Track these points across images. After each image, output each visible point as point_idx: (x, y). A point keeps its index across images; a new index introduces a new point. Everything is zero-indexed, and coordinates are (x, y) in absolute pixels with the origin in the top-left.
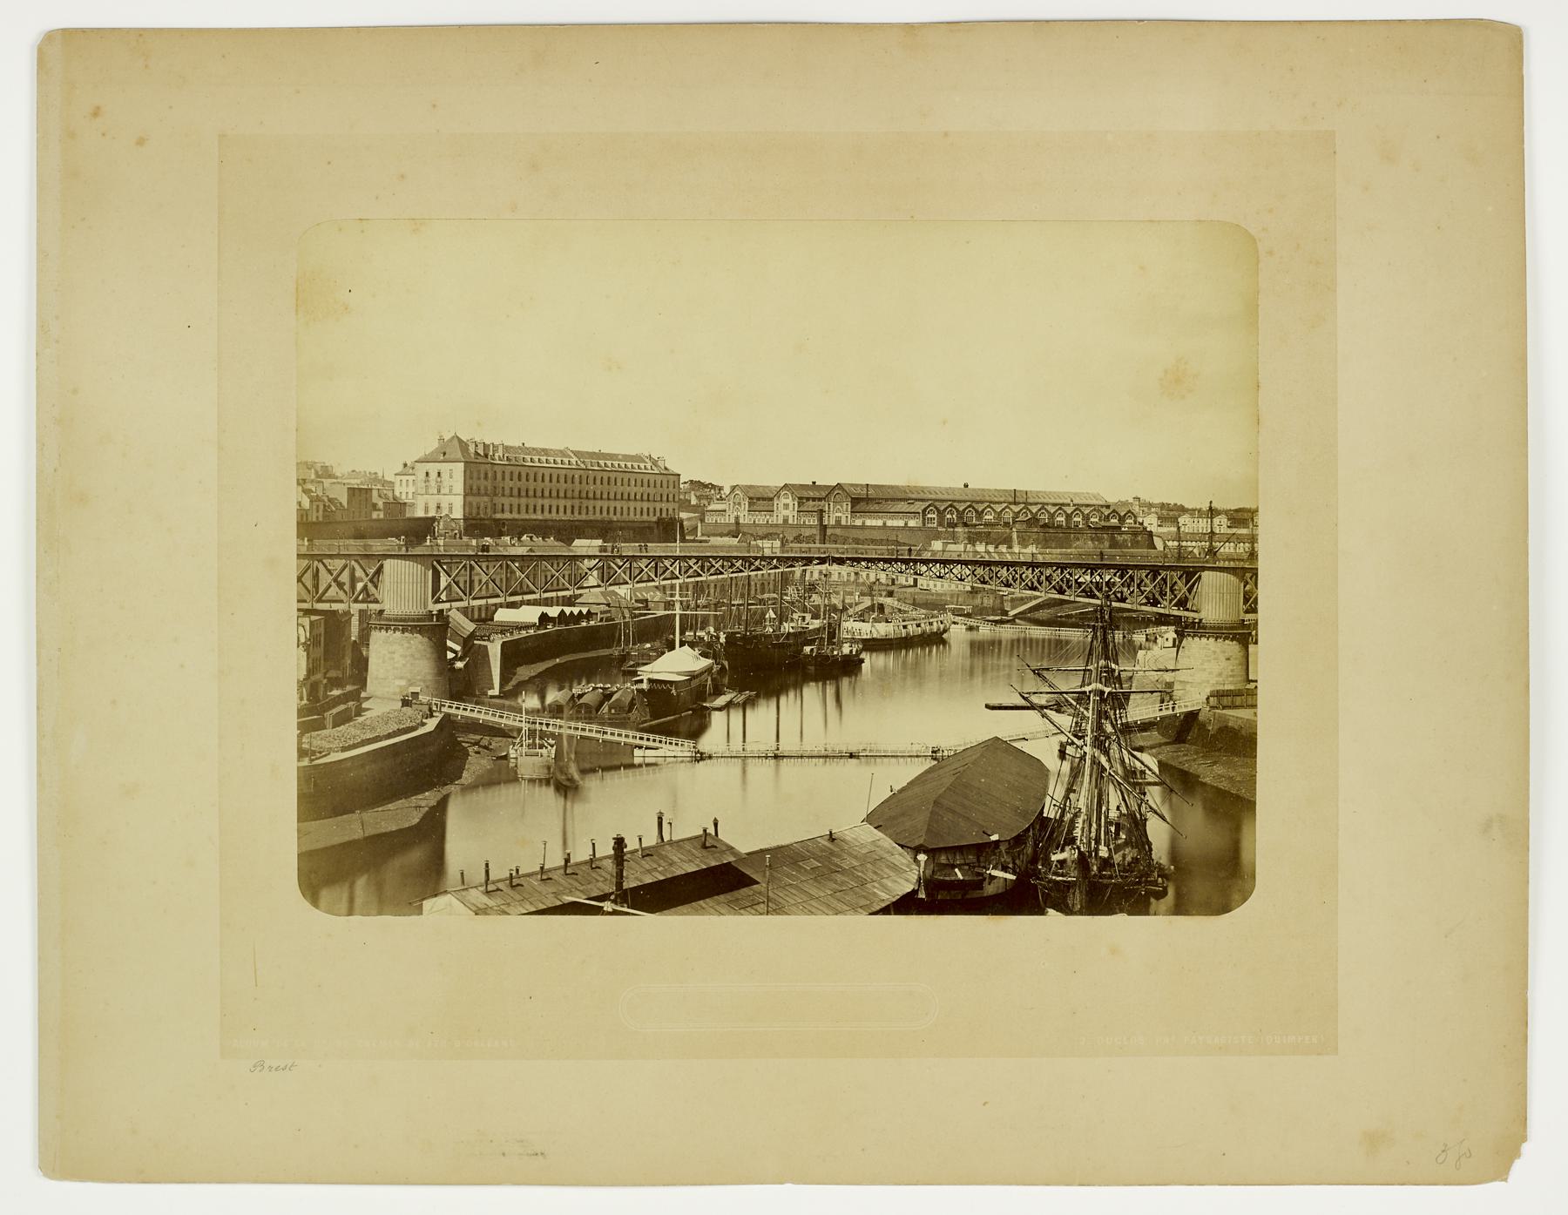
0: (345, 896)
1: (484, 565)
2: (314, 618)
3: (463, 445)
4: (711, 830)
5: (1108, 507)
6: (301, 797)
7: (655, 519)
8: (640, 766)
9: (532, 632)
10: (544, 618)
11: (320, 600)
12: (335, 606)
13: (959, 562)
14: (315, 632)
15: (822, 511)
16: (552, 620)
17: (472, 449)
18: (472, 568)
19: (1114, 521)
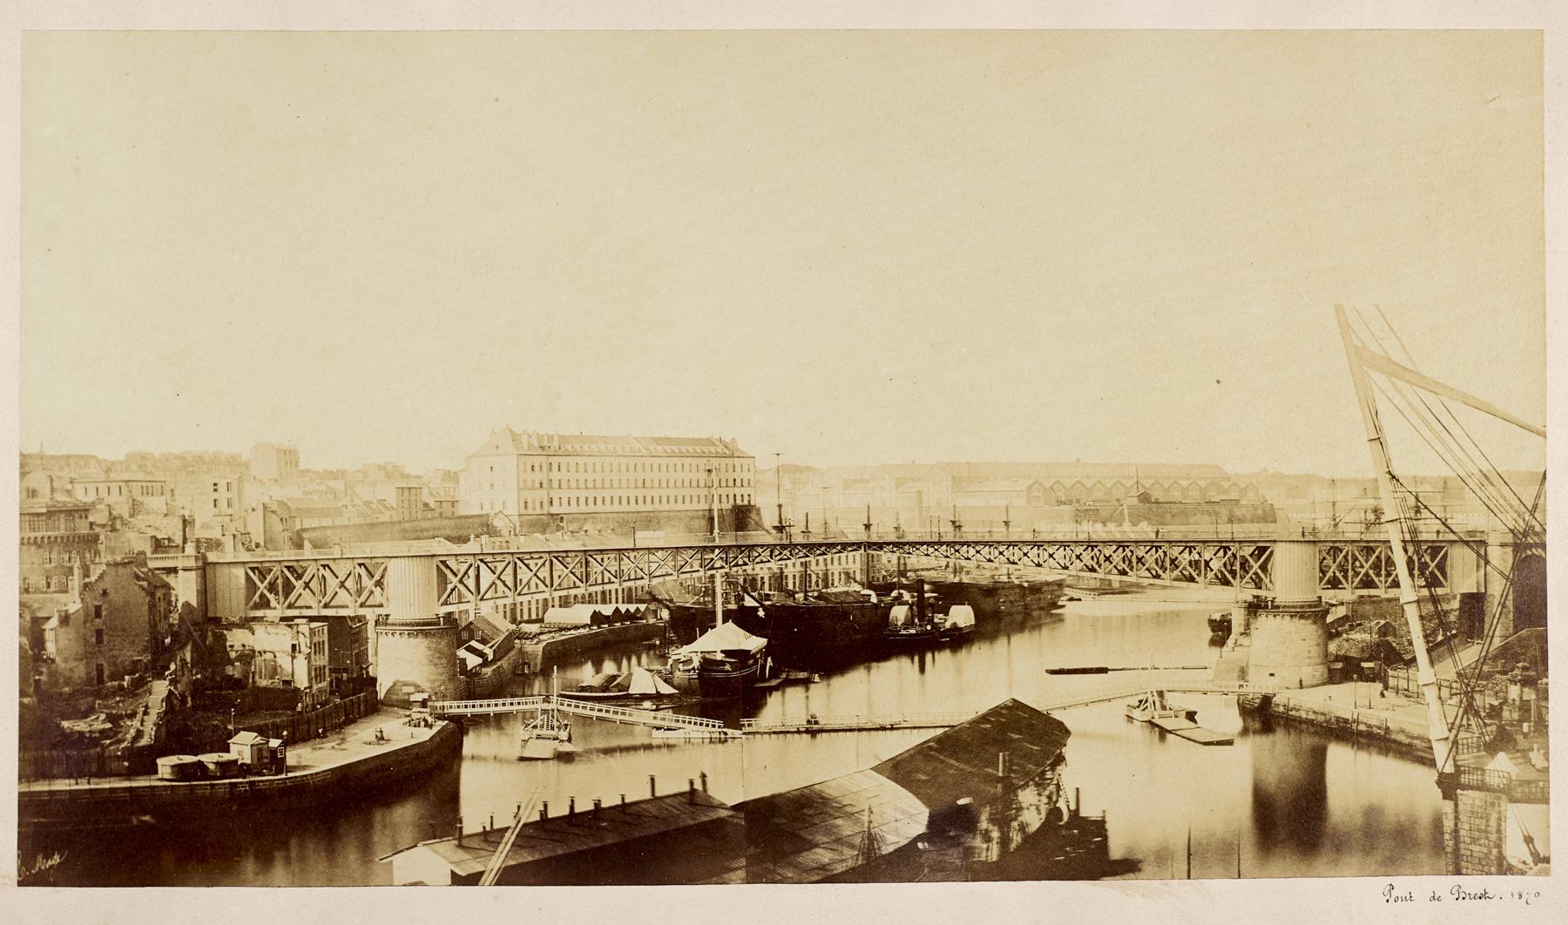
0: (225, 570)
1: (599, 558)
2: (314, 625)
3: (515, 437)
4: (698, 786)
5: (1229, 479)
6: (330, 883)
7: (729, 506)
8: (659, 747)
9: (582, 631)
10: (597, 618)
11: (326, 606)
12: (342, 613)
13: (986, 544)
14: (316, 639)
15: (920, 493)
16: (607, 619)
17: (525, 439)
18: (587, 563)
19: (1234, 495)
